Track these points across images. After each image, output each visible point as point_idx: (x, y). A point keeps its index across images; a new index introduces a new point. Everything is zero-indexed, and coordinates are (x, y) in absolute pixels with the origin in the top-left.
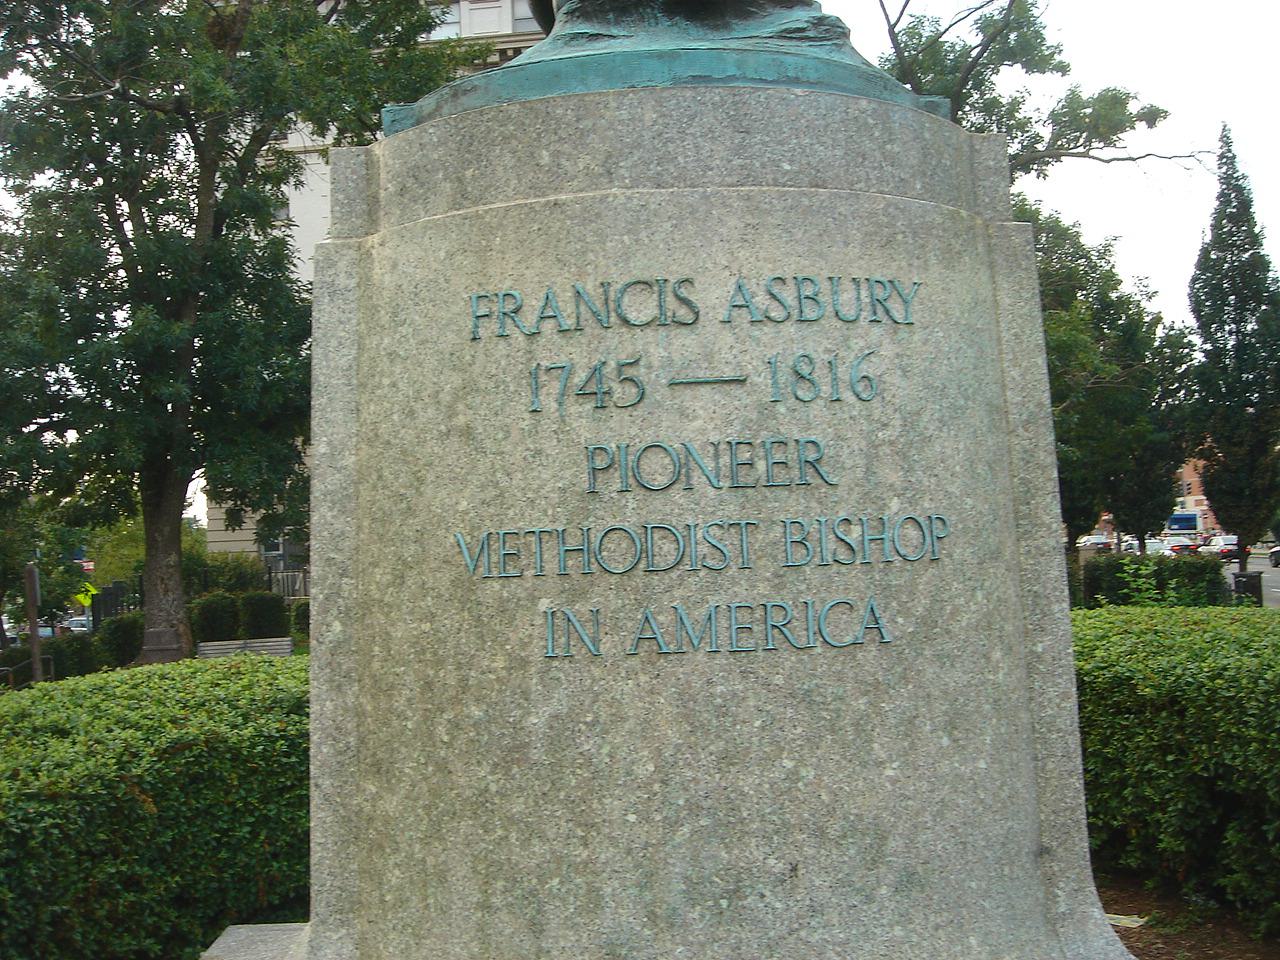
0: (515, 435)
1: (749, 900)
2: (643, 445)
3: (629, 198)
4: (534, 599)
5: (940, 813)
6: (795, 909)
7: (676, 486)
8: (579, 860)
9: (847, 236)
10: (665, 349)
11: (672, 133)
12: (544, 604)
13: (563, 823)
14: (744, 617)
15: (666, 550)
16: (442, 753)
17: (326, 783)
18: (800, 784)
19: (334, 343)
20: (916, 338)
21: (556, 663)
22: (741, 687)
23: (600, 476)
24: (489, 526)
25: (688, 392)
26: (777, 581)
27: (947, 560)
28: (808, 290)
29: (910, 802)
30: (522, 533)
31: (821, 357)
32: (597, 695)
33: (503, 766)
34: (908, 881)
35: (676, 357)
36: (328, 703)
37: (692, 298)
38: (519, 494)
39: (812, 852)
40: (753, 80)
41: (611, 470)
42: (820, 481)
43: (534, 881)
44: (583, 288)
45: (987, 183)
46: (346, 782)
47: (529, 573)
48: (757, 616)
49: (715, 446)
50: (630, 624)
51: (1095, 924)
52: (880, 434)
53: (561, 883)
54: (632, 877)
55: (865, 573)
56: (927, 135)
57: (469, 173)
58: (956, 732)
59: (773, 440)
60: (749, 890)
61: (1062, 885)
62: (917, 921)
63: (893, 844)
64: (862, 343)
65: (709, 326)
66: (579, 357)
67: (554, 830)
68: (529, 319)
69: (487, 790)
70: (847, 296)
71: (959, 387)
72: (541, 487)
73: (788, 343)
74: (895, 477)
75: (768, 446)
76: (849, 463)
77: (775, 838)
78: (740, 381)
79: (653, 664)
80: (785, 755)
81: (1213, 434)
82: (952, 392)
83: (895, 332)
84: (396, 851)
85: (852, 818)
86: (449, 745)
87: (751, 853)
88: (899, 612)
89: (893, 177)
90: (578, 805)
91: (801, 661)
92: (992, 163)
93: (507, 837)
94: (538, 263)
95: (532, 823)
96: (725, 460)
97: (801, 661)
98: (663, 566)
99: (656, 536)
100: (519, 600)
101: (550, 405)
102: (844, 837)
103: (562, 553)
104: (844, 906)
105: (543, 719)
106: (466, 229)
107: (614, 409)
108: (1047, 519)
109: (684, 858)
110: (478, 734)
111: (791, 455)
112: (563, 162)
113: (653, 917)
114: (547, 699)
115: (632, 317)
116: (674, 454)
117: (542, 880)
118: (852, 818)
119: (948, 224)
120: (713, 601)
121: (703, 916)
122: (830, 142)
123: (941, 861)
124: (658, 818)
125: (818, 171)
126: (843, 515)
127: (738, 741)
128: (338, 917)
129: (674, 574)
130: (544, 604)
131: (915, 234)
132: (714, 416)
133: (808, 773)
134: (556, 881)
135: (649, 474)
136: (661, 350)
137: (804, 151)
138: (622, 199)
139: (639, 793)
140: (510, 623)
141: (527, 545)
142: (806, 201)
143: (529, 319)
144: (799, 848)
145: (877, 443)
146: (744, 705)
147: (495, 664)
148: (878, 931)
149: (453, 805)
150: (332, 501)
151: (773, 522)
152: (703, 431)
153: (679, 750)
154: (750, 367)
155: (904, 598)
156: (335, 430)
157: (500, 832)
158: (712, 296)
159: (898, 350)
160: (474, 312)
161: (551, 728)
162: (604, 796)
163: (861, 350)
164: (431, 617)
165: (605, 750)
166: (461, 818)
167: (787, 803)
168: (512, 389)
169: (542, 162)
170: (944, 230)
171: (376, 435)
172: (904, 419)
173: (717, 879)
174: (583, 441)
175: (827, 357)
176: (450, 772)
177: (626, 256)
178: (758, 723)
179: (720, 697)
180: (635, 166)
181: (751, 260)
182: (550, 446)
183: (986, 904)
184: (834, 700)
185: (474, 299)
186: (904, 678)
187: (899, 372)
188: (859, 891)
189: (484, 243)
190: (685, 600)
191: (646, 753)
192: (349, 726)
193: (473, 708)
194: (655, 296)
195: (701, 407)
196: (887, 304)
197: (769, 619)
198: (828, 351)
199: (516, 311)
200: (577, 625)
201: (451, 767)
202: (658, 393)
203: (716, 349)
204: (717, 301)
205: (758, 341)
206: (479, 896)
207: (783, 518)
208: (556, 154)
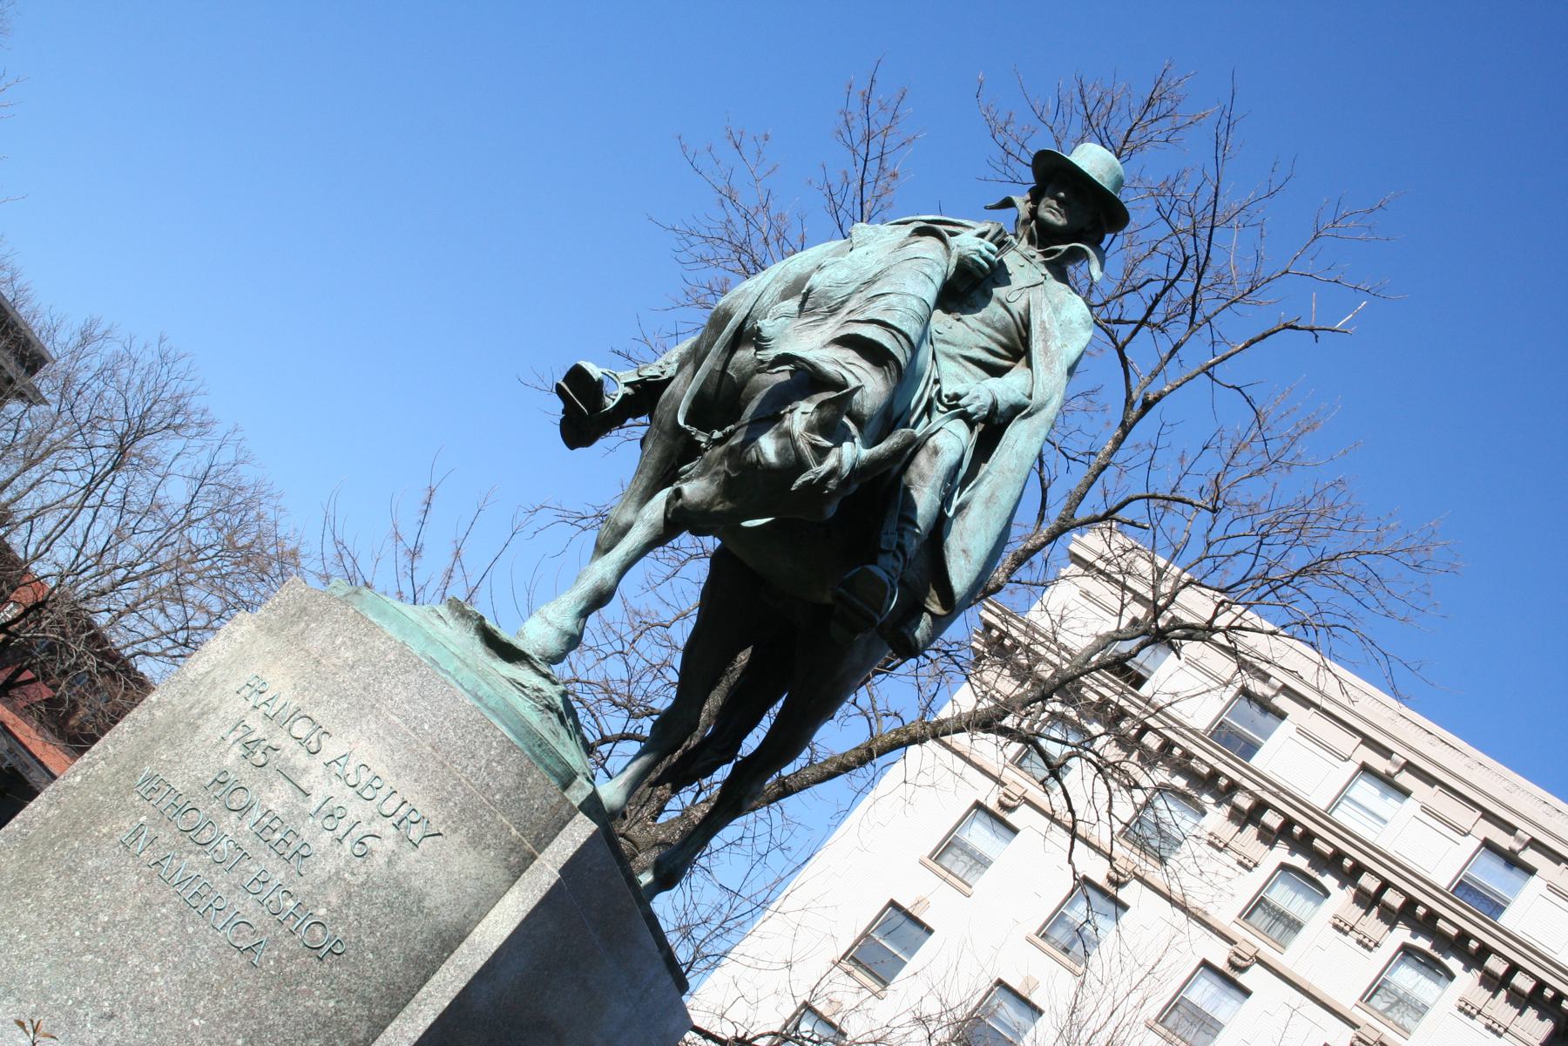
9: (420, 778)
11: (392, 672)
19: (206, 658)
20: (412, 854)
25: (282, 779)
35: (292, 760)
40: (457, 681)
45: (564, 842)
55: (276, 925)
64: (378, 828)
66: (259, 729)
68: (263, 698)
73: (343, 795)
74: (334, 901)
94: (288, 680)
96: (266, 820)
101: (231, 740)
129: (199, 848)
131: (463, 810)
142: (415, 746)
150: (134, 725)
155: (284, 956)
158: (331, 749)
180: (364, 673)
182: (213, 756)
198: (358, 816)
205: (331, 783)
208: (344, 643)
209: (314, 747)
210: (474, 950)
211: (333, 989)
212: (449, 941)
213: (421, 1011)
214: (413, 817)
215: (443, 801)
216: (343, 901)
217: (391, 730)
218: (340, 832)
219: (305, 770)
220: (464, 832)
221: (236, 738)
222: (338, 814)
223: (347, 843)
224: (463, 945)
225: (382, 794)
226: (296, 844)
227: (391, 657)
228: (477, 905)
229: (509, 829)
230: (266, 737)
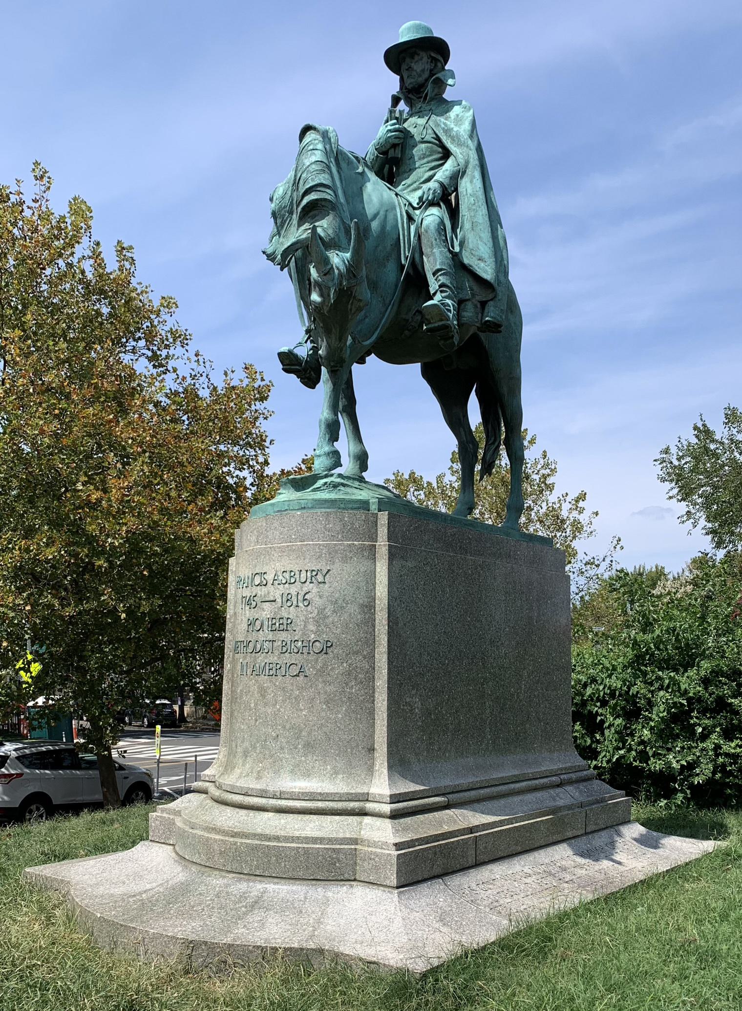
34: (307, 745)
63: (303, 733)
70: (303, 574)
78: (275, 601)
81: (7, 640)
96: (270, 623)
126: (296, 639)
152: (266, 615)
158: (270, 577)
209: (265, 582)
210: (380, 600)
212: (369, 607)
214: (314, 573)
217: (282, 550)
218: (295, 603)
220: (337, 561)
222: (290, 596)
223: (301, 604)
224: (377, 601)
225: (297, 576)
226: (285, 622)
228: (367, 583)
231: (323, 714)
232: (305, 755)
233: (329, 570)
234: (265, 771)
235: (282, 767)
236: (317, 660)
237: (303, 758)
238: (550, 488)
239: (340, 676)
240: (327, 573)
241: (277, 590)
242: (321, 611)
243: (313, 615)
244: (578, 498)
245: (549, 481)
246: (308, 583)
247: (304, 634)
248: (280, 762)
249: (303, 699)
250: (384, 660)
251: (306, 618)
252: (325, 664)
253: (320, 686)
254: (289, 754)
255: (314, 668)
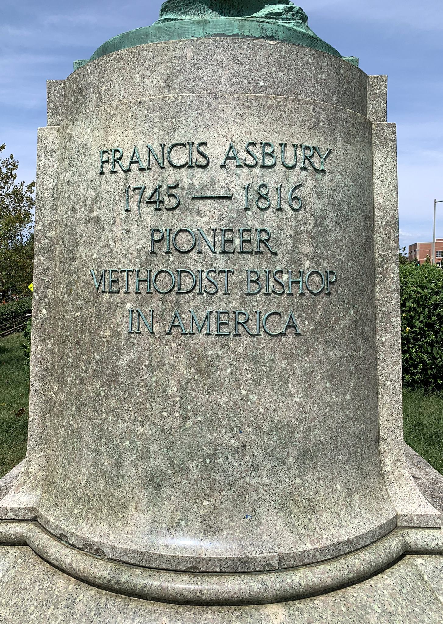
0: (118, 222)
1: (221, 459)
2: (178, 229)
3: (176, 99)
4: (124, 304)
5: (324, 421)
6: (244, 466)
7: (194, 251)
8: (139, 432)
10: (191, 179)
12: (129, 306)
13: (132, 414)
14: (224, 318)
15: (187, 282)
16: (82, 375)
17: (37, 384)
18: (249, 403)
20: (326, 178)
21: (133, 335)
22: (221, 352)
23: (157, 244)
24: (105, 267)
25: (202, 202)
26: (242, 300)
27: (334, 294)
28: (269, 150)
29: (307, 415)
30: (120, 271)
31: (272, 186)
32: (151, 352)
33: (107, 384)
35: (196, 183)
36: (39, 347)
37: (206, 152)
38: (119, 252)
39: (254, 437)
41: (162, 241)
42: (267, 251)
43: (119, 441)
44: (152, 147)
46: (46, 384)
47: (122, 291)
48: (231, 317)
49: (215, 230)
50: (168, 318)
51: (405, 478)
52: (302, 228)
53: (131, 443)
54: (164, 443)
56: (342, 72)
57: (103, 89)
58: (335, 381)
59: (244, 228)
60: (221, 455)
61: (389, 457)
62: (309, 476)
64: (295, 179)
65: (214, 167)
67: (128, 417)
68: (125, 163)
69: (100, 394)
71: (348, 206)
72: (129, 248)
74: (307, 250)
75: (241, 231)
76: (284, 242)
77: (235, 429)
78: (230, 198)
79: (179, 338)
80: (242, 387)
82: (344, 207)
83: (315, 175)
84: (63, 419)
85: (276, 421)
86: (85, 371)
87: (223, 436)
88: (306, 318)
89: (321, 92)
90: (140, 405)
91: (252, 341)
92: (378, 91)
93: (107, 418)
94: (131, 133)
95: (118, 413)
96: (219, 238)
97: (252, 341)
98: (185, 290)
99: (183, 275)
100: (117, 303)
101: (134, 206)
102: (271, 431)
103: (137, 281)
104: (270, 466)
105: (126, 362)
106: (99, 117)
107: (165, 210)
108: (392, 275)
109: (189, 436)
110: (97, 367)
111: (254, 236)
112: (146, 80)
113: (172, 465)
114: (128, 352)
115: (176, 162)
116: (193, 233)
117: (122, 441)
118: (276, 421)
119: (349, 119)
120: (209, 309)
121: (197, 466)
122: (286, 71)
123: (323, 445)
124: (178, 414)
125: (279, 87)
126: (278, 268)
127: (219, 379)
128: (40, 447)
129: (191, 295)
130: (129, 306)
131: (330, 123)
132: (214, 215)
133: (253, 397)
134: (128, 442)
135: (180, 244)
136: (189, 180)
137: (272, 75)
138: (173, 99)
139: (169, 402)
140: (113, 314)
141: (122, 277)
143: (125, 163)
144: (247, 435)
145: (300, 232)
146: (222, 361)
147: (106, 334)
148: (287, 480)
149: (85, 400)
150: (44, 253)
151: (242, 271)
152: (208, 223)
153: (189, 382)
154: (234, 190)
155: (310, 312)
156: (46, 219)
157: (104, 415)
159: (316, 184)
160: (101, 159)
161: (129, 367)
162: (152, 402)
163: (295, 183)
164: (80, 309)
165: (154, 379)
166: (89, 407)
167: (242, 412)
168: (117, 199)
169: (136, 81)
170: (347, 122)
171: (63, 221)
172: (316, 220)
173: (205, 448)
174: (149, 226)
175: (275, 186)
176: (85, 384)
177: (173, 129)
178: (228, 371)
179: (210, 356)
180: (181, 82)
181: (238, 132)
182: (134, 228)
183: (347, 468)
184: (269, 361)
185: (101, 153)
186: (307, 352)
187: (315, 196)
188: (278, 459)
189: (107, 124)
190: (196, 307)
191: (173, 382)
192: (49, 358)
193: (96, 354)
194: (187, 151)
195: (208, 210)
196: (312, 160)
197: (237, 319)
198: (276, 182)
199: (120, 158)
200: (143, 317)
201: (85, 382)
202: (186, 202)
203: (217, 180)
204: (219, 154)
206: (95, 445)
207: (247, 268)
208: (143, 76)
211: (347, 303)
213: (387, 269)
215: (315, 126)
216: (313, 246)
219: (213, 182)
221: (137, 203)
227: (190, 55)
229: (356, 114)
230: (158, 183)
231: (327, 398)
232: (301, 474)
233: (330, 152)
234: (220, 514)
235: (260, 502)
236: (315, 305)
237: (298, 480)
238: (14, 177)
239: (346, 331)
240: (328, 155)
241: (235, 178)
242: (320, 220)
243: (308, 227)
244: (31, 184)
245: (13, 173)
246: (298, 169)
247: (292, 260)
248: (253, 494)
249: (294, 374)
250: (393, 302)
251: (297, 232)
252: (327, 314)
253: (321, 350)
254: (270, 476)
255: (310, 318)
